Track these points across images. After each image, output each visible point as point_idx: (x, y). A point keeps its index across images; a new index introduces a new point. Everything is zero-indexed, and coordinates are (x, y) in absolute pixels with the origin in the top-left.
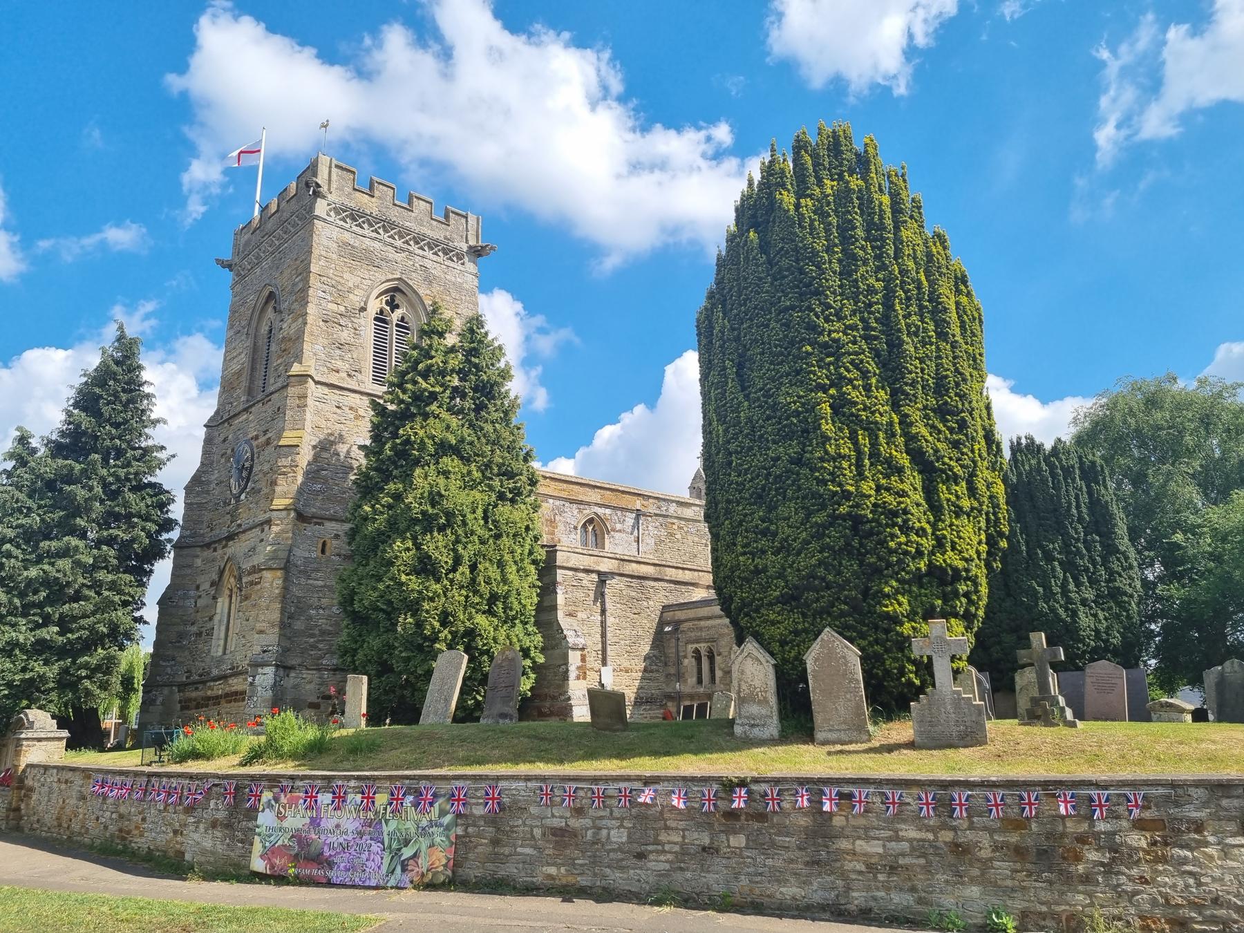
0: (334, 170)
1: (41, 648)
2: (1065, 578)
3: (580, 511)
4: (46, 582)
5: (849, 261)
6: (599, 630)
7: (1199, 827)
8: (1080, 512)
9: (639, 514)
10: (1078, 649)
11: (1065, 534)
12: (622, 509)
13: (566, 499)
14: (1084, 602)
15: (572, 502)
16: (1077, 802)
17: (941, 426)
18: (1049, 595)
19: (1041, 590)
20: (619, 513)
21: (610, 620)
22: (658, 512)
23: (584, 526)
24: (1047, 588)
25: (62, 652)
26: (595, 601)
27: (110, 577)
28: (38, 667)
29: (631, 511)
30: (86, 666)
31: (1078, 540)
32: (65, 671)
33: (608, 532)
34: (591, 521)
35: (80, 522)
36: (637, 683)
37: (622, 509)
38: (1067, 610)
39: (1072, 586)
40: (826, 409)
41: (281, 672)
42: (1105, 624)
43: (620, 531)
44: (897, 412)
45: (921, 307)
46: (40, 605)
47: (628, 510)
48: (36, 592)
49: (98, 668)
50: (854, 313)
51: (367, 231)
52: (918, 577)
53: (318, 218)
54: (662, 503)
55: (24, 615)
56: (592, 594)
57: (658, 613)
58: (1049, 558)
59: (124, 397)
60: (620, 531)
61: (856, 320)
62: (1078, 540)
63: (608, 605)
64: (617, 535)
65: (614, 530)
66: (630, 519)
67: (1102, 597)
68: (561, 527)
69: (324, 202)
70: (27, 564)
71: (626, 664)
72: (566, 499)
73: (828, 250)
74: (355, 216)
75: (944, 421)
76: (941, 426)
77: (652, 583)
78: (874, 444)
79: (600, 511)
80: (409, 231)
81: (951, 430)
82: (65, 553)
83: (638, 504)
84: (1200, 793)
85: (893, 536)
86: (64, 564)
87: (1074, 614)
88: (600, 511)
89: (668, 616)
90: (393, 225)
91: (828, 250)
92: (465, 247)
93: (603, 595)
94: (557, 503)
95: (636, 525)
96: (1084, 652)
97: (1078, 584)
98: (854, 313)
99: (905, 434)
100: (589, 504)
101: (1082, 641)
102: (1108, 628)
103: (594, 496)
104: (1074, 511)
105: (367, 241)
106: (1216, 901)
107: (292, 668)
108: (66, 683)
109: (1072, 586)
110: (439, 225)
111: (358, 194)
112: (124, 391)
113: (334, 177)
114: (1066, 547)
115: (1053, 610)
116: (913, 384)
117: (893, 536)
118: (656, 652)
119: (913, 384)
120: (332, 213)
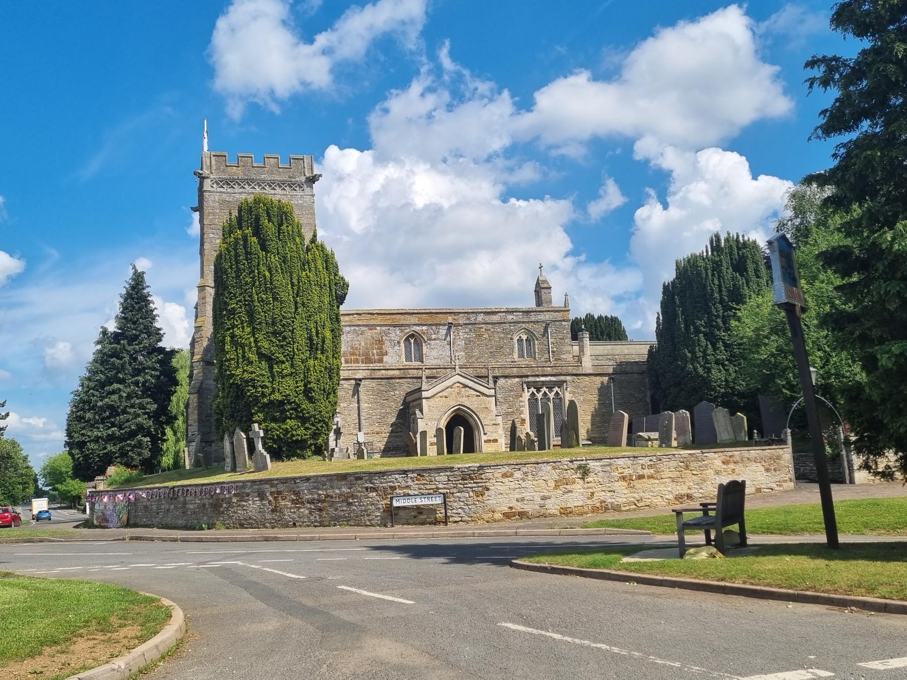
0: (213, 159)
1: (111, 438)
2: (707, 346)
3: (402, 331)
4: (111, 407)
5: (238, 272)
6: (357, 412)
7: (248, 495)
8: (721, 295)
9: (450, 325)
10: (711, 395)
11: (709, 313)
12: (436, 325)
13: (390, 325)
14: (717, 362)
15: (395, 326)
16: (222, 488)
17: (274, 340)
18: (694, 359)
19: (689, 355)
20: (434, 328)
21: (364, 405)
22: (467, 322)
23: (407, 340)
24: (693, 353)
25: (121, 439)
26: (353, 395)
27: (137, 401)
28: (110, 447)
29: (444, 325)
30: (130, 445)
31: (717, 316)
32: (121, 448)
33: (425, 342)
34: (412, 336)
35: (120, 376)
36: (386, 440)
37: (436, 325)
38: (705, 368)
39: (710, 351)
40: (228, 339)
41: (204, 445)
42: (734, 375)
43: (435, 339)
44: (254, 335)
45: (266, 288)
46: (108, 417)
47: (440, 325)
48: (105, 412)
49: (135, 446)
50: (241, 294)
51: (237, 189)
52: (265, 405)
53: (205, 191)
54: (471, 316)
55: (103, 423)
56: (351, 392)
57: (403, 398)
58: (697, 331)
59: (137, 307)
60: (435, 339)
61: (241, 297)
62: (717, 316)
63: (361, 397)
64: (433, 342)
65: (430, 339)
66: (443, 331)
67: (734, 357)
68: (387, 344)
69: (209, 180)
70: (102, 398)
71: (378, 429)
72: (390, 325)
73: (231, 267)
74: (228, 182)
75: (276, 337)
76: (274, 340)
77: (398, 381)
78: (244, 352)
79: (417, 328)
80: (264, 181)
81: (279, 341)
82: (113, 392)
83: (450, 319)
84: (249, 484)
85: (249, 390)
86: (115, 397)
87: (709, 370)
88: (417, 328)
89: (409, 399)
90: (253, 181)
91: (231, 267)
92: (303, 179)
93: (358, 391)
94: (384, 328)
95: (448, 333)
96: (717, 397)
97: (715, 349)
98: (241, 294)
99: (256, 346)
100: (408, 325)
101: (714, 389)
102: (735, 379)
103: (413, 320)
104: (716, 295)
105: (237, 196)
106: (250, 518)
107: (213, 441)
108: (124, 454)
109: (710, 351)
110: (284, 170)
111: (229, 169)
112: (136, 303)
113: (213, 162)
114: (709, 324)
115: (695, 369)
116: (260, 323)
117: (249, 390)
118: (401, 421)
119: (260, 323)
120: (215, 186)
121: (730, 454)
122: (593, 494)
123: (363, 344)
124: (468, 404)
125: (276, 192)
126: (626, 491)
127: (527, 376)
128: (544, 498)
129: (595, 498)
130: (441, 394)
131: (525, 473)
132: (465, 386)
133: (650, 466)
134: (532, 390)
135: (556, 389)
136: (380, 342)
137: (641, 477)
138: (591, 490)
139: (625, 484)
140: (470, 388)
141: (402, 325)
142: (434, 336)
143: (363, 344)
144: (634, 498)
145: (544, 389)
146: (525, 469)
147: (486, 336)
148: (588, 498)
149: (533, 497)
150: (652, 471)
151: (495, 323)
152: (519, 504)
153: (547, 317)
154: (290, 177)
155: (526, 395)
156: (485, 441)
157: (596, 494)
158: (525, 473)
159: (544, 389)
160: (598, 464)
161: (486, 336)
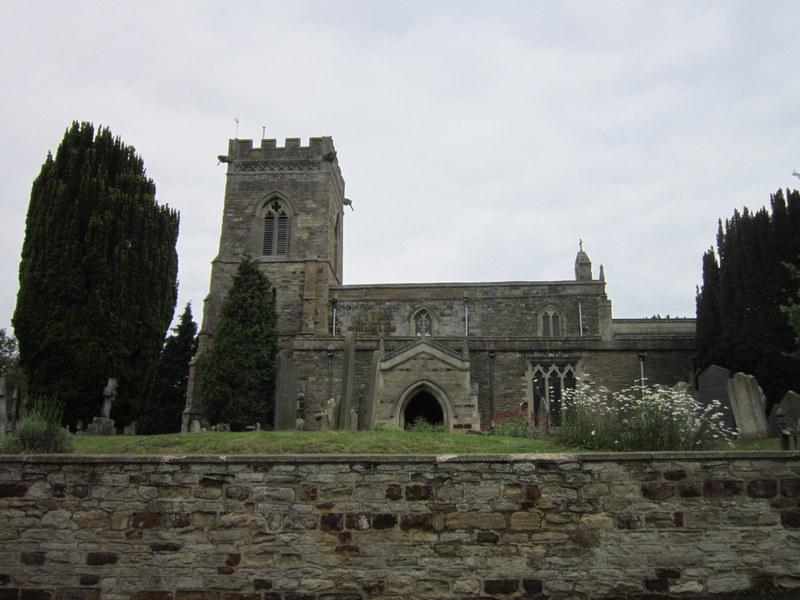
80: (282, 163)
90: (273, 163)
92: (320, 158)
121: (668, 467)
122: (234, 559)
123: (370, 319)
124: (434, 379)
125: (284, 172)
126: (333, 559)
127: (532, 351)
128: (96, 559)
129: (239, 571)
130: (400, 367)
131: (59, 489)
132: (433, 357)
133: (415, 494)
134: (539, 367)
135: (568, 368)
136: (389, 317)
137: (383, 522)
138: (231, 549)
139: (331, 537)
140: (439, 359)
141: (413, 300)
142: (447, 312)
143: (370, 319)
144: (356, 579)
145: (554, 367)
146: (58, 478)
147: (506, 312)
148: (221, 571)
149: (68, 553)
150: (422, 507)
151: (516, 298)
152: (27, 569)
153: (578, 291)
154: (308, 157)
155: (530, 375)
156: (455, 427)
157: (245, 561)
158: (59, 489)
159: (554, 367)
160: (259, 476)
161: (506, 312)
